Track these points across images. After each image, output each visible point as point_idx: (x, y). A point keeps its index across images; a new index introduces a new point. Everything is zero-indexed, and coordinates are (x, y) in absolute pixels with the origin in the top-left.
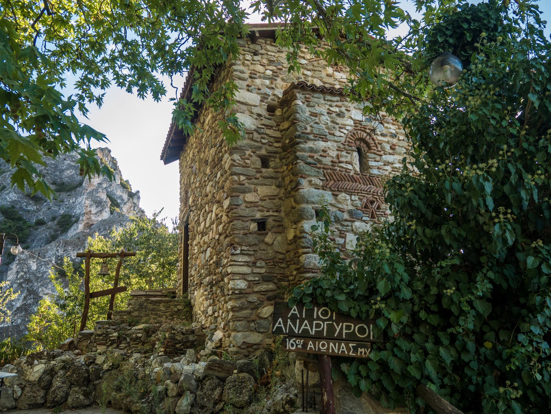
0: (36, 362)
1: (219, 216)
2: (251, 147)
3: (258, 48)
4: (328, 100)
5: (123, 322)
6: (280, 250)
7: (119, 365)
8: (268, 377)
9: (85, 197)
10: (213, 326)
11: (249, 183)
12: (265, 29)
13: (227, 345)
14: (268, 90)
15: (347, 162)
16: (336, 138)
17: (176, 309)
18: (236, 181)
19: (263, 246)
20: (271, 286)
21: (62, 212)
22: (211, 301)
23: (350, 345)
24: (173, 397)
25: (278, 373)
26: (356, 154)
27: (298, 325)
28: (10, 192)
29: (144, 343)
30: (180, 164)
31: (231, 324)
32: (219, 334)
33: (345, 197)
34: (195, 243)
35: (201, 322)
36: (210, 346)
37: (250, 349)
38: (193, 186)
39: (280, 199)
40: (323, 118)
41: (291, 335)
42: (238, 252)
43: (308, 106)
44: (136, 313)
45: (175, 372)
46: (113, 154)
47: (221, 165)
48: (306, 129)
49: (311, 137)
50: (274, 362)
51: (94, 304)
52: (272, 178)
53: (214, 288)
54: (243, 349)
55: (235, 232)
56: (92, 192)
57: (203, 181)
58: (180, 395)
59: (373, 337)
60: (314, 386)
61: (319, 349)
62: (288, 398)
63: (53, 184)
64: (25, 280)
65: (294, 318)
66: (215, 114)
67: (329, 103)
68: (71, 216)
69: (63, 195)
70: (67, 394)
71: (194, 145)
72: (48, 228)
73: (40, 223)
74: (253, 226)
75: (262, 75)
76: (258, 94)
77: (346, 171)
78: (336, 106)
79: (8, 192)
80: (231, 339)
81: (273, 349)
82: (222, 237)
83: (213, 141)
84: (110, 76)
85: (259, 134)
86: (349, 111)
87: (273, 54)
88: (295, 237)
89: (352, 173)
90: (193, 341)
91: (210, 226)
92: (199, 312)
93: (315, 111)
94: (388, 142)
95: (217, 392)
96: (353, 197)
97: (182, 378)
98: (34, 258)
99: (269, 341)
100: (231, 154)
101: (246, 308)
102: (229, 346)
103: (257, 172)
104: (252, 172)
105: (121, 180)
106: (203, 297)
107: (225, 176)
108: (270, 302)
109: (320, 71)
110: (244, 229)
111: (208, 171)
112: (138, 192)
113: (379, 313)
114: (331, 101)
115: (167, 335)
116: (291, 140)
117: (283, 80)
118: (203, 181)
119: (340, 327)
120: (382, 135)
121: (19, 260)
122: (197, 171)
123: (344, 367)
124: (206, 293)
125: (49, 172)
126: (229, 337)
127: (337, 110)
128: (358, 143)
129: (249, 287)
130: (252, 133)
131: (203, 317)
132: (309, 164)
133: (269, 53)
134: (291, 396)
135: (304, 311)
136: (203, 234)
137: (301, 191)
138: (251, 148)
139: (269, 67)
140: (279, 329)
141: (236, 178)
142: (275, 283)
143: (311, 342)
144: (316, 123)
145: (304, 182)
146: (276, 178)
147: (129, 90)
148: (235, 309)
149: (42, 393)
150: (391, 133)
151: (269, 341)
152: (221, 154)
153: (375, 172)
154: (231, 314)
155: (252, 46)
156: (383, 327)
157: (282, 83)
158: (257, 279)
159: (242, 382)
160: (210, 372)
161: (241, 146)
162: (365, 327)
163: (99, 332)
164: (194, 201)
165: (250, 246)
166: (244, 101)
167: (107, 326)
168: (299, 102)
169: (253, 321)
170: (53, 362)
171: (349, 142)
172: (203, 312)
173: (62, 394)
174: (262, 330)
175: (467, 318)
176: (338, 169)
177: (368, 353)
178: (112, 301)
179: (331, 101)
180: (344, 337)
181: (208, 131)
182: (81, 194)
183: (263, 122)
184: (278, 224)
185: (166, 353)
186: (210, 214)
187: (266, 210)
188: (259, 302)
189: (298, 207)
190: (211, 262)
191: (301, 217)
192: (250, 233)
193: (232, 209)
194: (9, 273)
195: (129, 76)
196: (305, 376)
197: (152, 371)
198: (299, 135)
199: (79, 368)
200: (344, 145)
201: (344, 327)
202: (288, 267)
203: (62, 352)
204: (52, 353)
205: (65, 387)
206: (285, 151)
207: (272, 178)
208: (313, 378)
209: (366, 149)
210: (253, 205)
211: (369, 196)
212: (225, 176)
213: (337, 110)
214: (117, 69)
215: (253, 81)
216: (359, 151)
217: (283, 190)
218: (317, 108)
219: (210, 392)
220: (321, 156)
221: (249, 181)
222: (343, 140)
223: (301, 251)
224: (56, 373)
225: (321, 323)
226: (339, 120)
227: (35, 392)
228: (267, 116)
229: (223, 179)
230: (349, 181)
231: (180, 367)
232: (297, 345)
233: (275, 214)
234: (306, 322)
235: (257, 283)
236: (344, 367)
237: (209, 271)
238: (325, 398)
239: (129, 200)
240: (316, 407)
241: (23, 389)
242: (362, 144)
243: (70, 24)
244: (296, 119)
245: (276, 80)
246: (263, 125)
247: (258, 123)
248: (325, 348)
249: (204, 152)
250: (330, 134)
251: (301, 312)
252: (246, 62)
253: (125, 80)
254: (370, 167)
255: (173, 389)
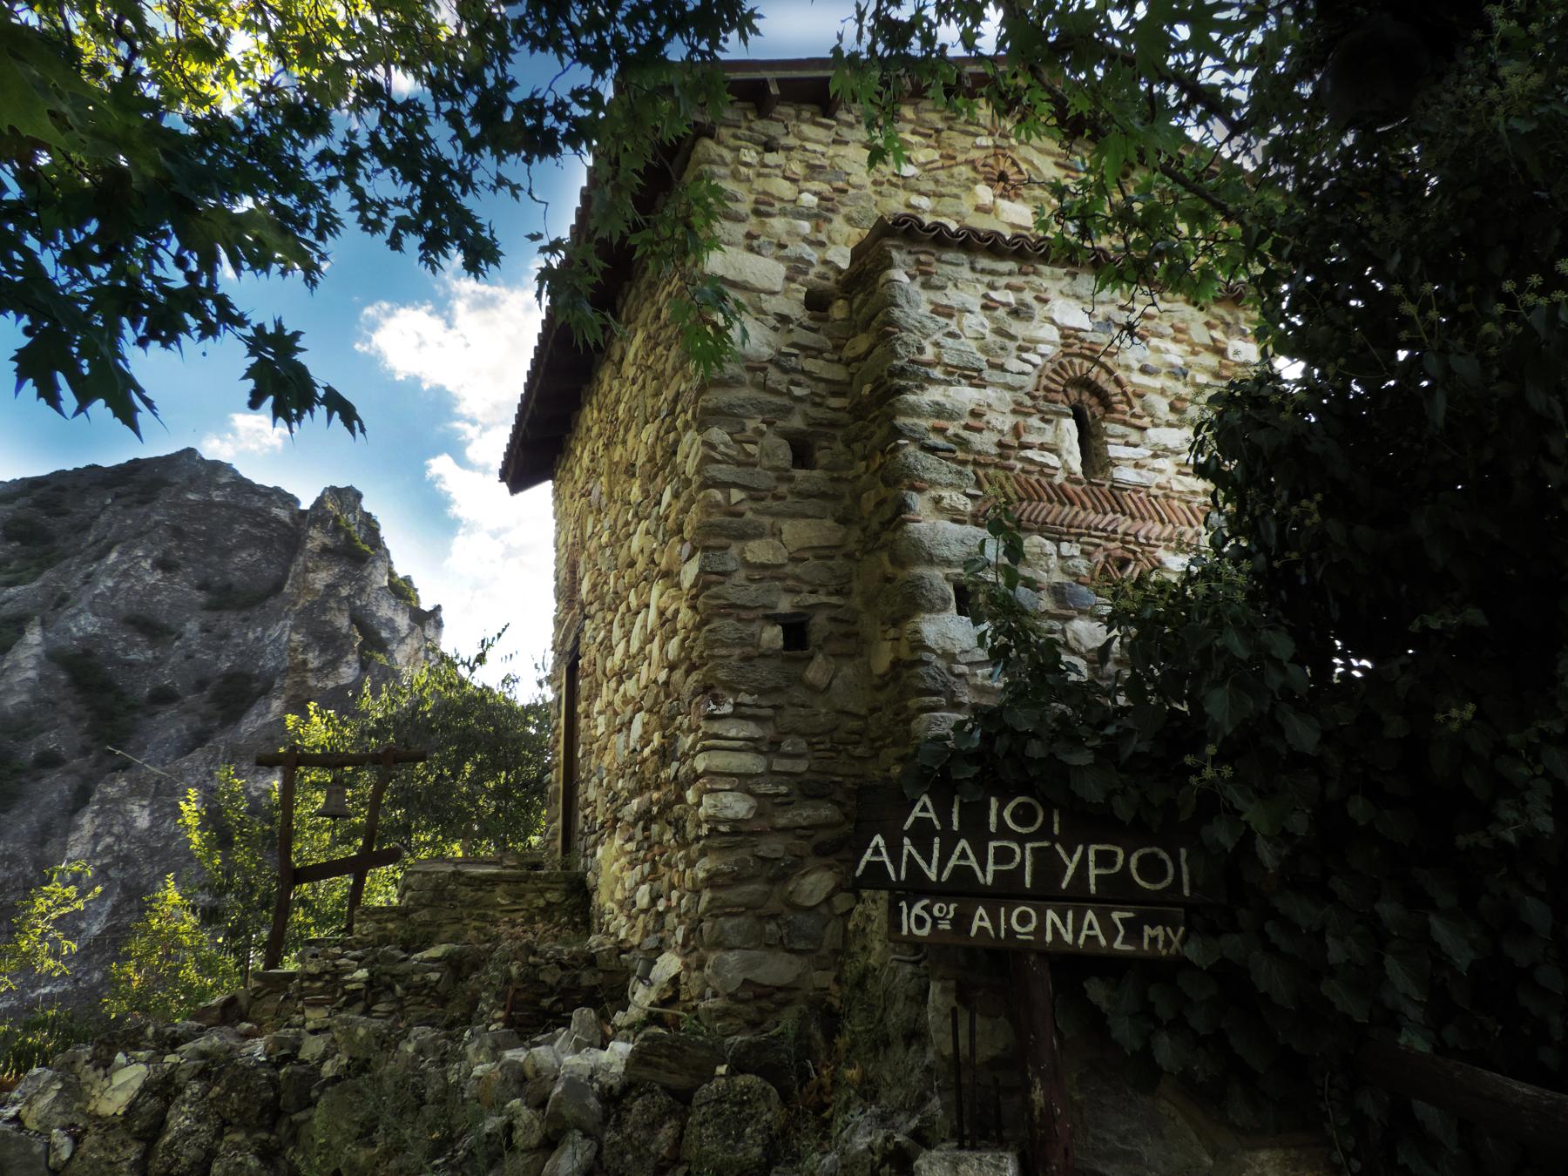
0: (120, 1058)
1: (669, 614)
2: (760, 408)
3: (775, 129)
4: (983, 271)
5: (385, 940)
6: (851, 707)
7: (368, 1061)
8: (821, 1088)
9: (289, 623)
10: (651, 942)
11: (756, 512)
12: (795, 74)
13: (695, 992)
14: (808, 249)
15: (1042, 447)
16: (1009, 378)
17: (542, 903)
18: (717, 505)
19: (798, 695)
20: (826, 812)
21: (225, 666)
22: (647, 867)
23: (1116, 916)
24: (528, 1150)
25: (852, 1074)
26: (1069, 425)
27: (936, 854)
28: (81, 611)
29: (443, 1001)
30: (556, 491)
31: (706, 926)
32: (669, 964)
33: (1042, 546)
34: (598, 705)
35: (616, 934)
36: (642, 997)
37: (764, 1004)
38: (592, 545)
39: (849, 556)
40: (968, 320)
41: (917, 887)
42: (727, 709)
43: (926, 286)
44: (424, 915)
45: (537, 1073)
46: (366, 505)
47: (674, 468)
48: (921, 350)
49: (937, 373)
50: (842, 1042)
51: (303, 902)
52: (823, 495)
53: (655, 828)
54: (743, 1001)
55: (717, 652)
56: (306, 611)
57: (620, 523)
58: (550, 1144)
59: (1193, 887)
60: (994, 1063)
61: (1011, 932)
62: (890, 1146)
63: (200, 588)
64: (118, 859)
65: (922, 834)
66: (652, 329)
67: (987, 279)
68: (248, 678)
69: (229, 619)
70: (211, 1154)
71: (595, 430)
72: (186, 712)
73: (163, 697)
74: (772, 636)
75: (789, 207)
76: (778, 258)
77: (1042, 473)
78: (1008, 287)
79: (73, 611)
80: (707, 971)
81: (836, 1003)
82: (678, 675)
83: (650, 402)
84: (341, 200)
85: (785, 371)
86: (1045, 301)
87: (819, 148)
88: (896, 664)
89: (1059, 479)
90: (593, 989)
91: (642, 649)
92: (610, 905)
93: (945, 302)
94: (1163, 392)
95: (667, 1132)
96: (1065, 547)
97: (558, 1089)
98: (143, 795)
99: (823, 979)
100: (702, 427)
101: (751, 879)
102: (702, 997)
103: (779, 479)
104: (764, 479)
105: (392, 574)
106: (623, 860)
107: (684, 496)
108: (823, 861)
109: (956, 196)
110: (741, 642)
111: (636, 493)
112: (438, 608)
113: (1211, 804)
114: (992, 272)
115: (514, 970)
116: (878, 383)
117: (849, 220)
118: (620, 523)
119: (1076, 857)
120: (1144, 370)
121: (102, 801)
122: (604, 500)
123: (1096, 991)
124: (631, 846)
125: (191, 555)
126: (700, 967)
127: (1010, 297)
128: (1074, 393)
129: (759, 814)
130: (764, 369)
131: (623, 920)
132: (933, 450)
133: (809, 146)
134: (899, 1138)
135: (956, 810)
136: (622, 675)
137: (911, 526)
138: (762, 412)
139: (809, 185)
140: (876, 869)
141: (718, 495)
142: (839, 804)
143: (981, 911)
144: (951, 335)
145: (919, 503)
146: (837, 498)
147: (395, 243)
148: (720, 881)
149: (133, 1152)
150: (1172, 366)
151: (823, 979)
152: (672, 436)
153: (1126, 474)
154: (706, 896)
155: (759, 125)
156: (1230, 847)
157: (847, 229)
158: (783, 789)
159: (743, 1103)
160: (645, 1073)
161: (730, 406)
162: (1164, 855)
163: (312, 968)
164: (594, 587)
165: (762, 692)
166: (738, 278)
167: (338, 950)
168: (899, 275)
169: (773, 917)
170: (171, 1059)
171: (1047, 389)
172: (621, 905)
173: (192, 1153)
174: (800, 945)
175: (1525, 803)
176: (1019, 465)
177: (1176, 940)
178: (356, 891)
179: (992, 272)
180: (1093, 888)
181: (634, 382)
182: (278, 616)
183: (795, 338)
184: (843, 629)
185: (509, 1022)
186: (641, 616)
187: (806, 588)
188: (789, 859)
189: (902, 575)
190: (647, 751)
191: (914, 601)
192: (762, 656)
193: (707, 586)
194: (72, 838)
195: (397, 203)
196: (963, 1032)
197: (468, 1075)
198: (903, 369)
199: (249, 1072)
200: (1033, 398)
201: (1092, 857)
202: (877, 756)
203: (201, 1030)
204: (169, 1030)
205: (205, 1132)
206: (862, 418)
207: (823, 495)
208: (992, 1039)
209: (1099, 411)
210: (768, 573)
211: (1112, 545)
212: (684, 496)
213: (1010, 297)
214: (361, 182)
215: (763, 224)
216: (1079, 416)
217: (856, 533)
218: (951, 290)
219: (643, 1134)
220: (967, 427)
221: (754, 506)
222: (1030, 383)
223: (913, 703)
224: (180, 1091)
225: (1015, 846)
226: (1016, 327)
227: (113, 1150)
228: (807, 322)
229: (681, 504)
230: (1050, 500)
231: (551, 1059)
232: (935, 920)
233: (834, 600)
234: (963, 843)
235: (786, 803)
236: (1096, 991)
237: (640, 782)
238: (1038, 1095)
239: (412, 629)
240: (1005, 1134)
241: (77, 1140)
242: (1086, 396)
243: (228, 57)
244: (893, 323)
245: (830, 221)
246: (794, 345)
247: (780, 341)
248: (1031, 927)
249: (624, 442)
250: (992, 366)
251: (945, 816)
252: (743, 169)
253: (383, 209)
254: (1112, 463)
255: (529, 1127)
